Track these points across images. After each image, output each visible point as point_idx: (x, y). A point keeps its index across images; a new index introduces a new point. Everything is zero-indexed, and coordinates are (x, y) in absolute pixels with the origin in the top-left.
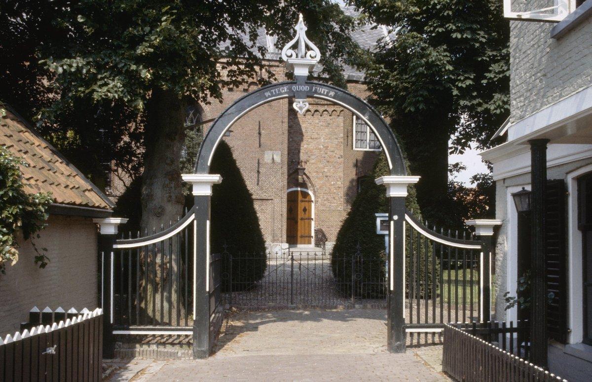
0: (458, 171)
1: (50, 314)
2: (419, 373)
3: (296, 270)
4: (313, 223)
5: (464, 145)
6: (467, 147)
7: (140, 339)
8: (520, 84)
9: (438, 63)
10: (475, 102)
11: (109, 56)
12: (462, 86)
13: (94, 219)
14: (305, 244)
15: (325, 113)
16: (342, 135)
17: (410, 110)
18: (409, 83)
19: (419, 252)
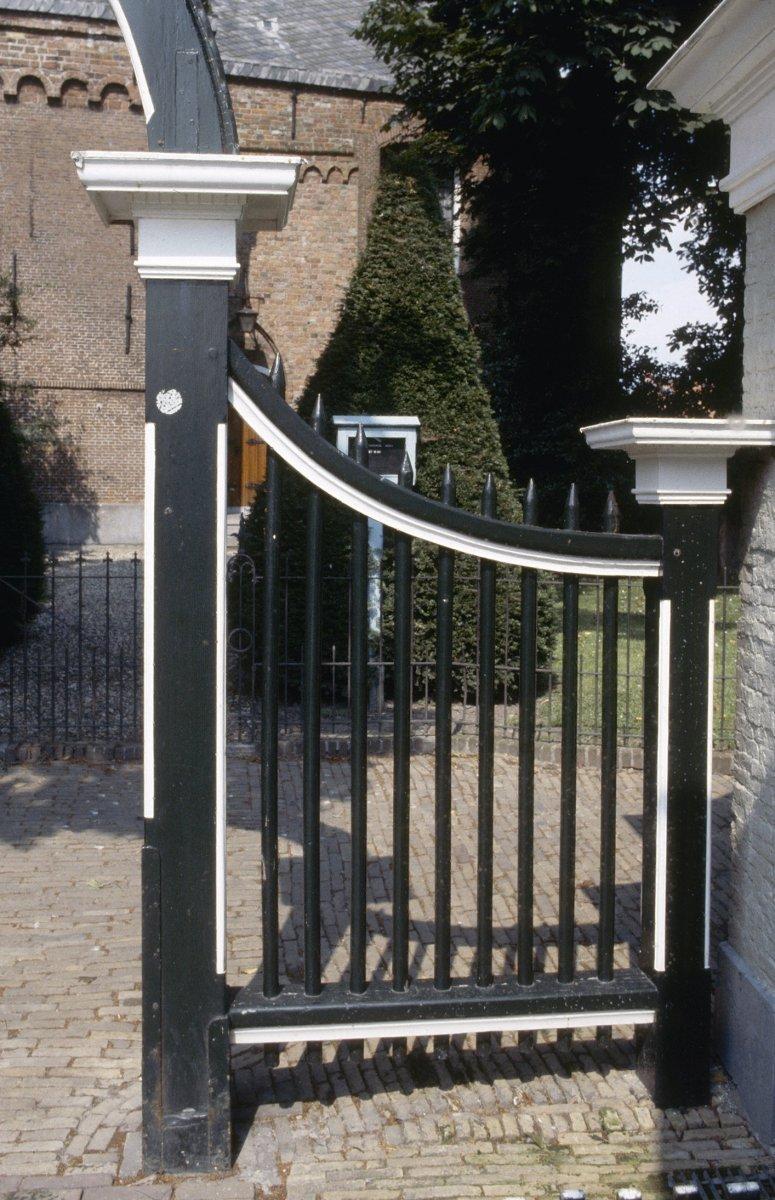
12: (639, 56)
15: (313, 174)
16: (354, 232)
17: (491, 126)
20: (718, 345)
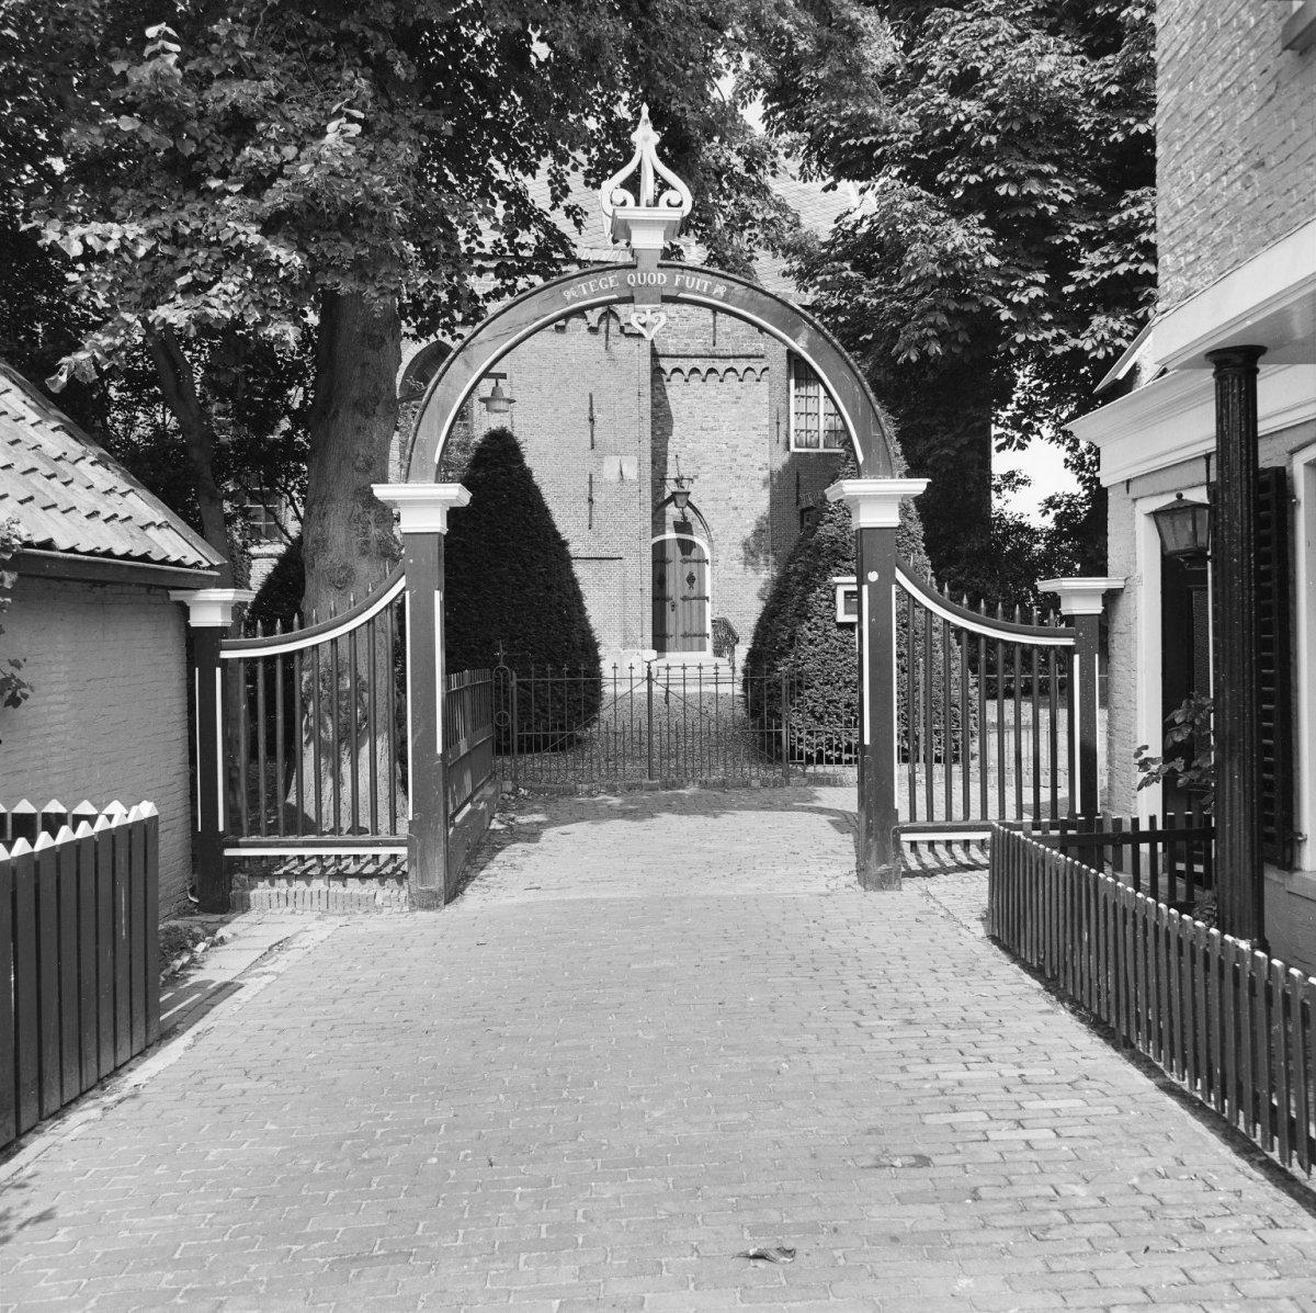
0: (1013, 489)
1: (33, 816)
2: (932, 941)
3: (658, 703)
4: (708, 606)
5: (1028, 431)
6: (1033, 434)
7: (266, 869)
8: (1185, 207)
9: (967, 251)
10: (1048, 335)
11: (203, 216)
12: (1020, 302)
13: (171, 592)
14: (691, 650)
15: (731, 373)
16: (766, 421)
18: (906, 299)
19: (929, 656)
20: (1082, 511)
